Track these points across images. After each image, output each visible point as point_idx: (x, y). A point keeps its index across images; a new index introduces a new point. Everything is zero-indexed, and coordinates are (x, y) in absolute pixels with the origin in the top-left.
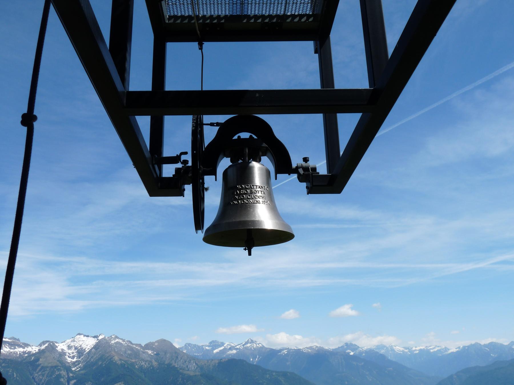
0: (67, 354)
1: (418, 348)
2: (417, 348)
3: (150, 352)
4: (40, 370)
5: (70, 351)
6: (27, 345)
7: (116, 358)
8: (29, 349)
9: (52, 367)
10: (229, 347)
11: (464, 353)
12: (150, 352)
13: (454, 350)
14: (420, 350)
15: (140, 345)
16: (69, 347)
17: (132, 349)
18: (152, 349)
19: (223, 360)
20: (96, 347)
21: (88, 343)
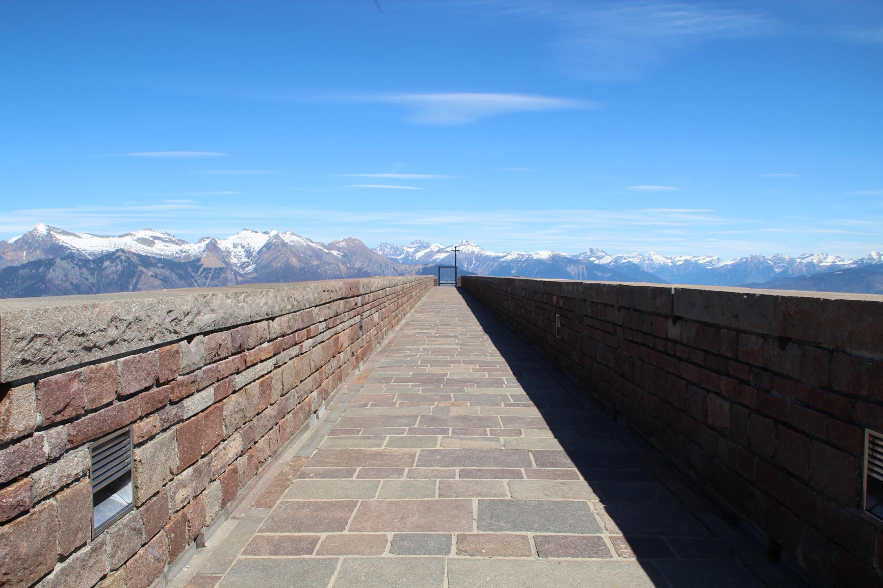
0: (233, 253)
1: (683, 258)
2: (680, 260)
3: (335, 253)
4: (202, 272)
5: (236, 250)
6: (184, 242)
7: (294, 261)
8: (185, 247)
9: (216, 269)
10: (437, 249)
11: (617, 269)
12: (335, 253)
13: (729, 262)
14: (686, 261)
15: (323, 245)
16: (235, 246)
17: (313, 250)
18: (339, 249)
19: (430, 265)
20: (268, 246)
21: (258, 241)
